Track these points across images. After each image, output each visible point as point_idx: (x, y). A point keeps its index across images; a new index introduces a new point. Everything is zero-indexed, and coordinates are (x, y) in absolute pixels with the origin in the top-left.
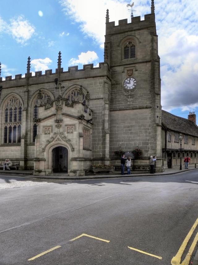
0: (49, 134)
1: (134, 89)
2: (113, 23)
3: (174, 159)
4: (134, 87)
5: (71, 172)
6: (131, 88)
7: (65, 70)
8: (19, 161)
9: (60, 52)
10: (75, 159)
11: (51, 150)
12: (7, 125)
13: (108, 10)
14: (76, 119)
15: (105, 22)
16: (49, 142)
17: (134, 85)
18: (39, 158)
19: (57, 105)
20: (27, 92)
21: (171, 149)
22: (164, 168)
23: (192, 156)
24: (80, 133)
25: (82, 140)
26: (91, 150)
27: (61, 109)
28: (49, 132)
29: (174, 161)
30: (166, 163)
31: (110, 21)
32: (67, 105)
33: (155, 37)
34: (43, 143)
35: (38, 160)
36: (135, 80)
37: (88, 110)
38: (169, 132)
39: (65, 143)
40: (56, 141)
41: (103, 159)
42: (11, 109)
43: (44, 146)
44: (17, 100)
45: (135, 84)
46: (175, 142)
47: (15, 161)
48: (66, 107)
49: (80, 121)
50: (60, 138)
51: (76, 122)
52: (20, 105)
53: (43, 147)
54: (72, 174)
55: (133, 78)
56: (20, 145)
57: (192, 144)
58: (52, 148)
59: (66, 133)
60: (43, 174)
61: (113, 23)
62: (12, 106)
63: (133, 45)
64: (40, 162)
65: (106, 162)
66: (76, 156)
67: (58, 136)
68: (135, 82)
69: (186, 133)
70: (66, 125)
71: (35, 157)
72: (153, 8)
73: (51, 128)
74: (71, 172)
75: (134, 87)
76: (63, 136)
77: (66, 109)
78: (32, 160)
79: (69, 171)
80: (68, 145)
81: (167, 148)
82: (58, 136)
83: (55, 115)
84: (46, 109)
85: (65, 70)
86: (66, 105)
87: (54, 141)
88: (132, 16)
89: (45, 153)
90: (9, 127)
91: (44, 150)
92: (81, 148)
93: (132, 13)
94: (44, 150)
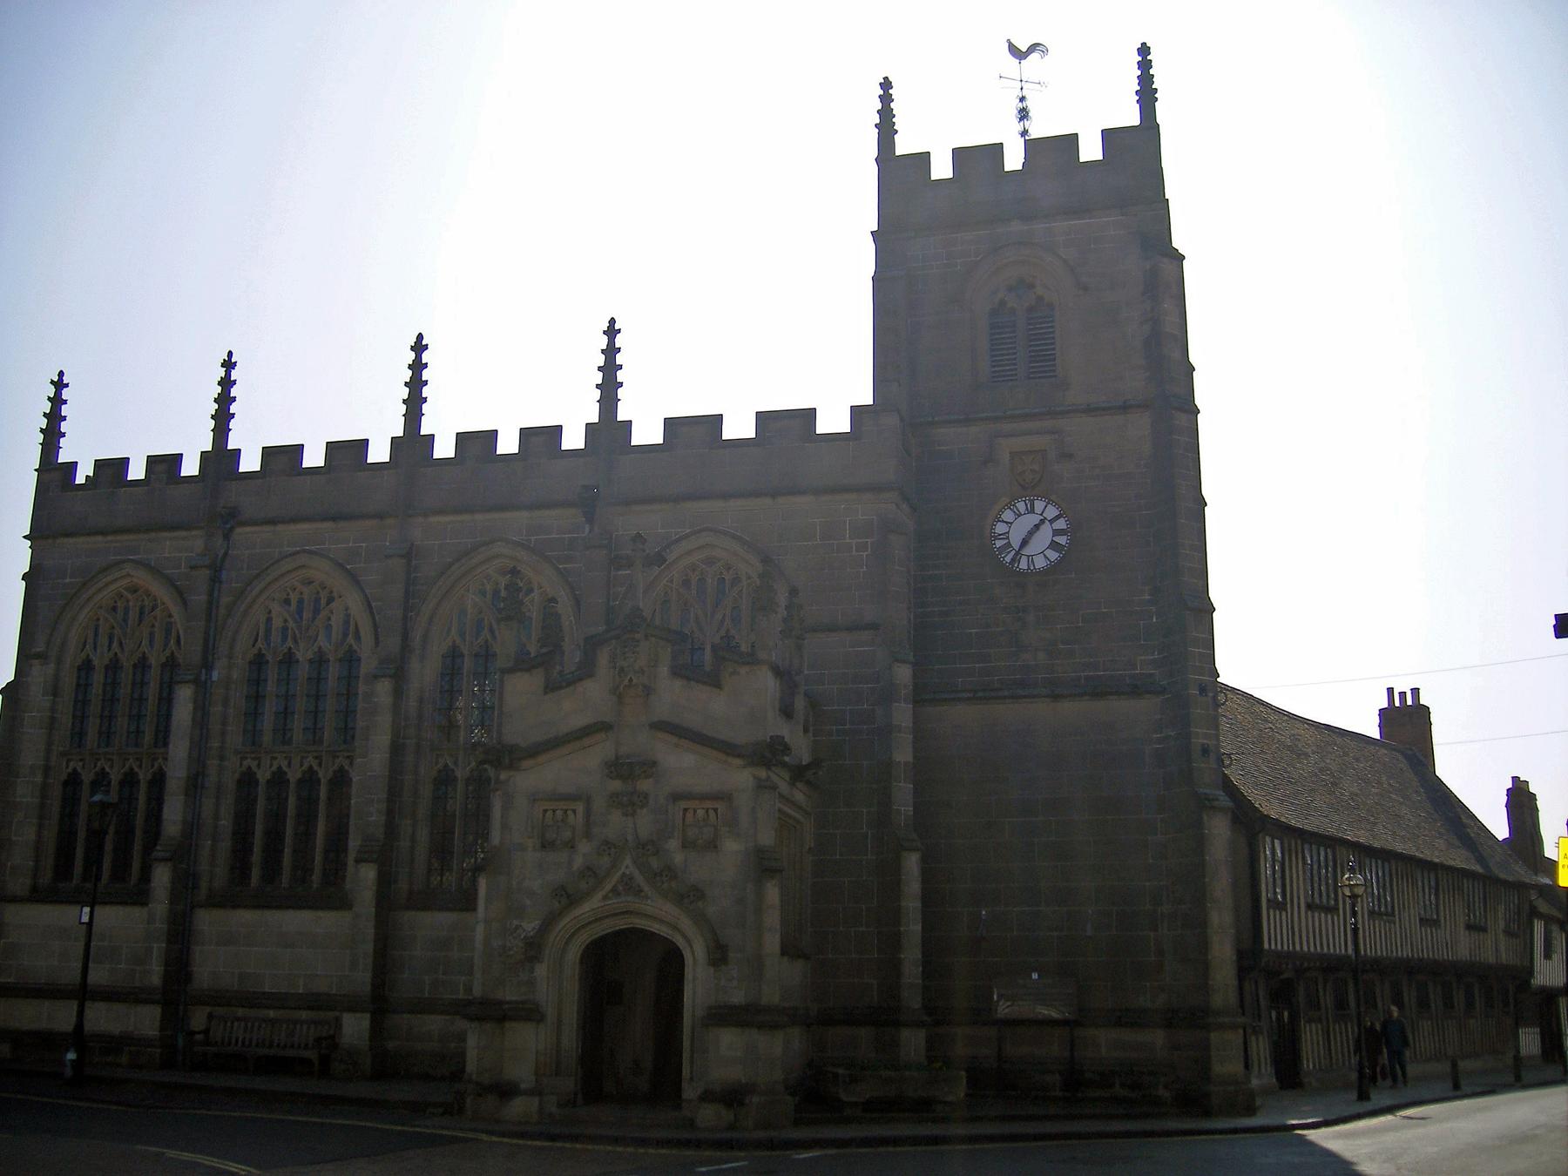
0: (571, 845)
1: (1053, 568)
2: (923, 159)
3: (1310, 1021)
4: (1053, 555)
5: (707, 1097)
6: (1040, 563)
7: (647, 432)
8: (331, 1014)
9: (612, 321)
10: (723, 1016)
11: (574, 953)
12: (254, 765)
13: (886, 85)
14: (738, 762)
15: (873, 151)
16: (567, 897)
17: (1054, 546)
18: (500, 1003)
19: (622, 670)
20: (402, 556)
21: (1290, 955)
22: (1255, 1082)
23: (1423, 1004)
24: (172, 617)
25: (772, 893)
26: (806, 957)
27: (648, 691)
28: (568, 834)
29: (1311, 1040)
30: (1261, 1047)
31: (903, 146)
32: (687, 672)
33: (1167, 265)
34: (528, 902)
35: (493, 1013)
36: (1058, 518)
37: (800, 703)
38: (1268, 839)
39: (669, 909)
40: (614, 890)
41: (885, 1017)
42: (289, 660)
43: (537, 923)
44: (330, 600)
45: (1062, 540)
46: (1309, 907)
47: (304, 1015)
48: (678, 683)
49: (763, 773)
50: (639, 879)
51: (741, 778)
52: (351, 640)
53: (530, 926)
54: (709, 1116)
55: (1049, 502)
56: (341, 902)
57: (1424, 922)
58: (585, 938)
59: (673, 844)
60: (519, 1107)
61: (923, 159)
62: (121, 644)
63: (1040, 299)
64: (507, 1025)
65: (905, 1033)
66: (737, 998)
67: (628, 861)
68: (1061, 524)
69: (1376, 845)
70: (676, 797)
71: (477, 991)
72: (1147, 95)
73: (580, 808)
74: (707, 1097)
75: (1053, 555)
76: (655, 863)
77: (672, 696)
78: (424, 1007)
79: (689, 1092)
80: (686, 923)
81: (1266, 946)
82: (628, 865)
83: (603, 727)
84: (550, 688)
85: (647, 432)
86: (676, 672)
87: (600, 895)
88: (1024, 133)
89: (541, 970)
90: (268, 775)
91: (533, 949)
92: (772, 943)
93: (1022, 99)
94: (533, 949)
